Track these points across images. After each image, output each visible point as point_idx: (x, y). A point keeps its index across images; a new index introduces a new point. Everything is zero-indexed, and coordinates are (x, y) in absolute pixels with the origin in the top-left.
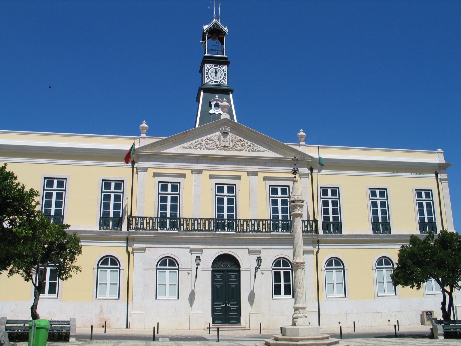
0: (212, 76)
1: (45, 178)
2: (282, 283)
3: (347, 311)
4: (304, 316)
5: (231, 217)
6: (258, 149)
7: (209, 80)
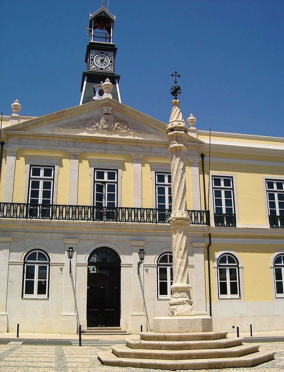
0: (97, 63)
1: (212, 176)
2: (228, 281)
3: (241, 314)
5: (46, 203)
7: (94, 66)
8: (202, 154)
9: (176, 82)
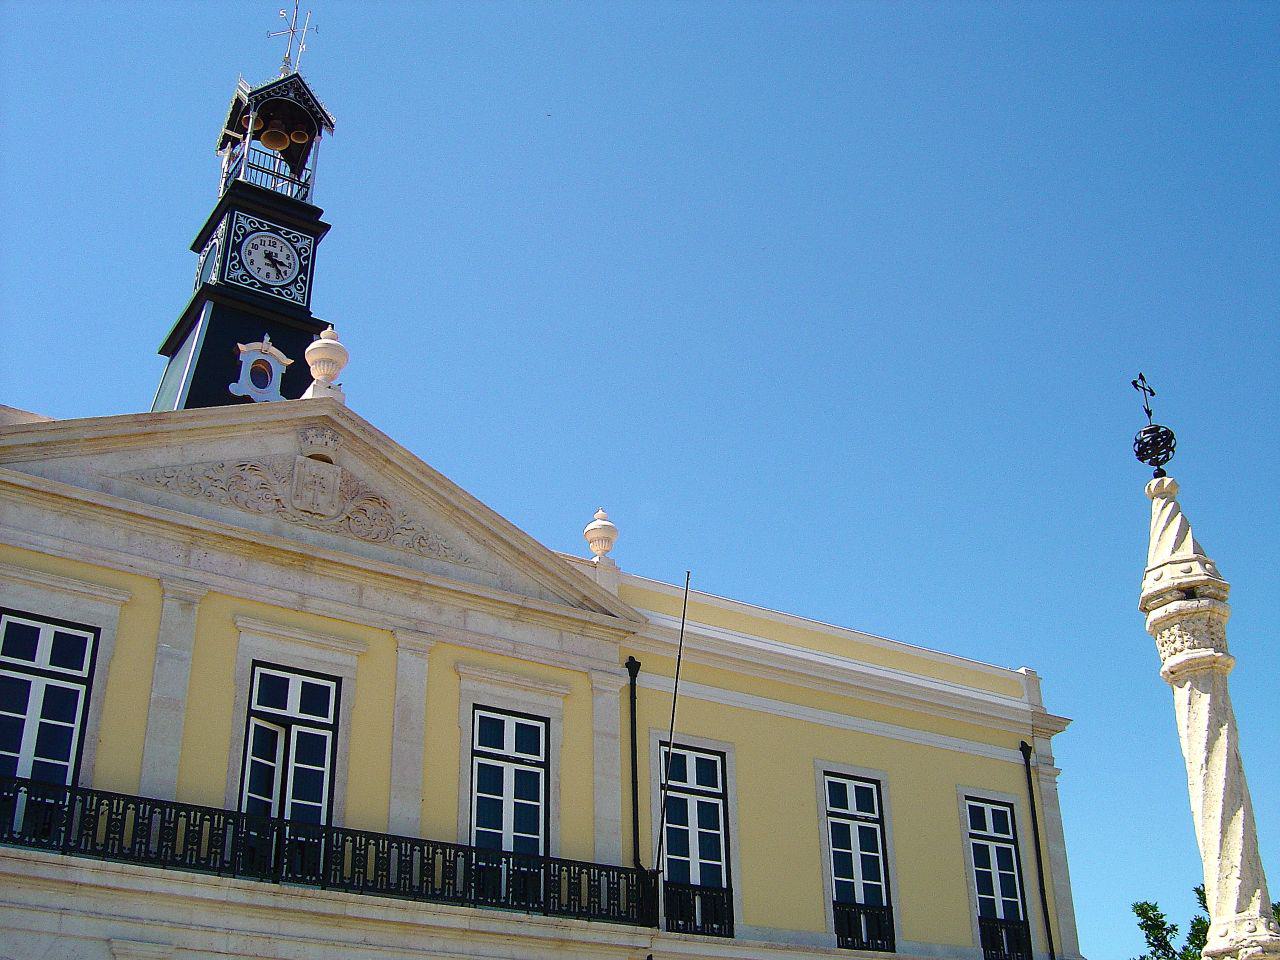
0: (252, 261)
8: (631, 658)
9: (1149, 413)
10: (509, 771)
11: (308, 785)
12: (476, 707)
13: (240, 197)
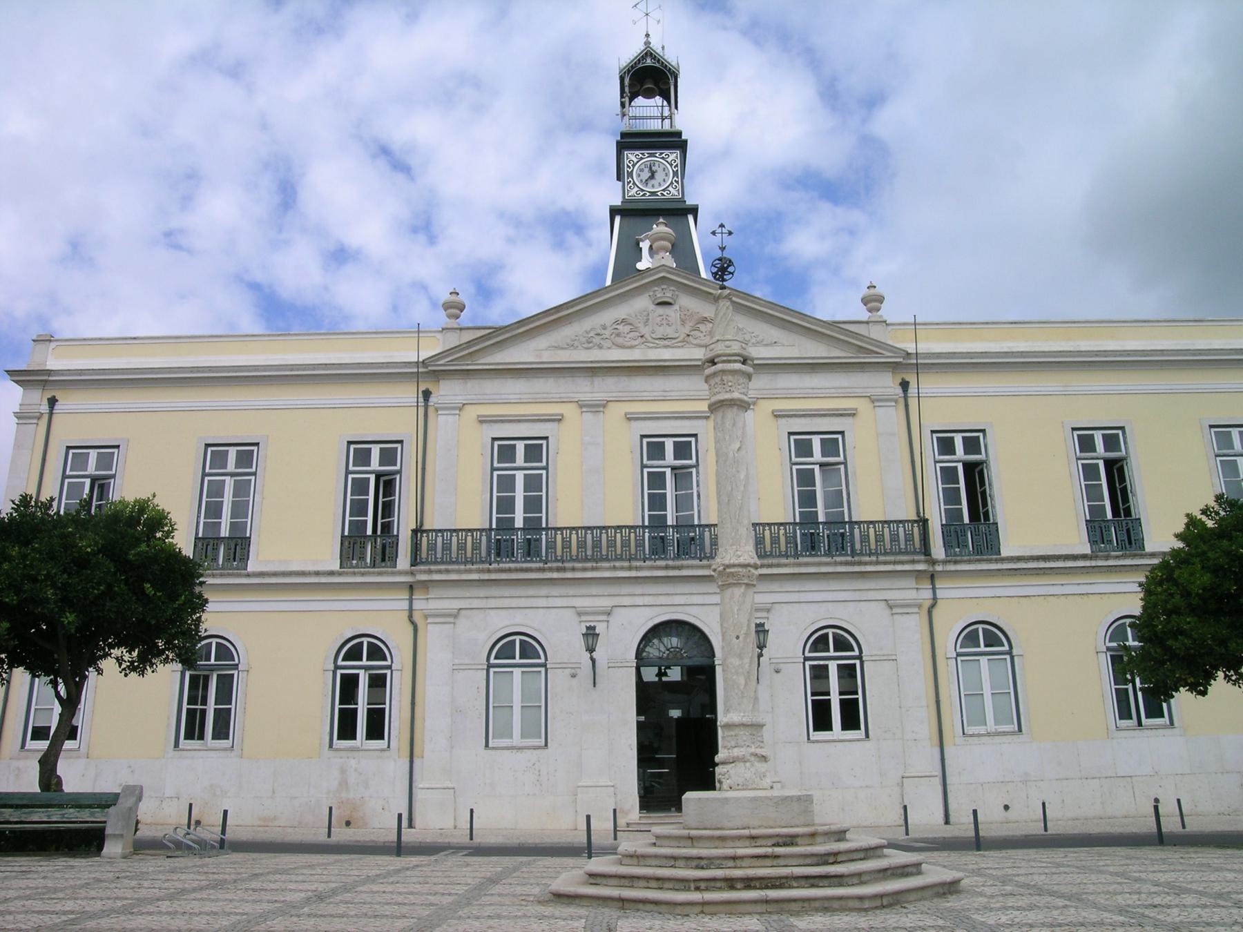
4: (752, 754)
6: (754, 340)
10: (520, 477)
11: (835, 499)
12: (1074, 429)
13: (630, 141)
